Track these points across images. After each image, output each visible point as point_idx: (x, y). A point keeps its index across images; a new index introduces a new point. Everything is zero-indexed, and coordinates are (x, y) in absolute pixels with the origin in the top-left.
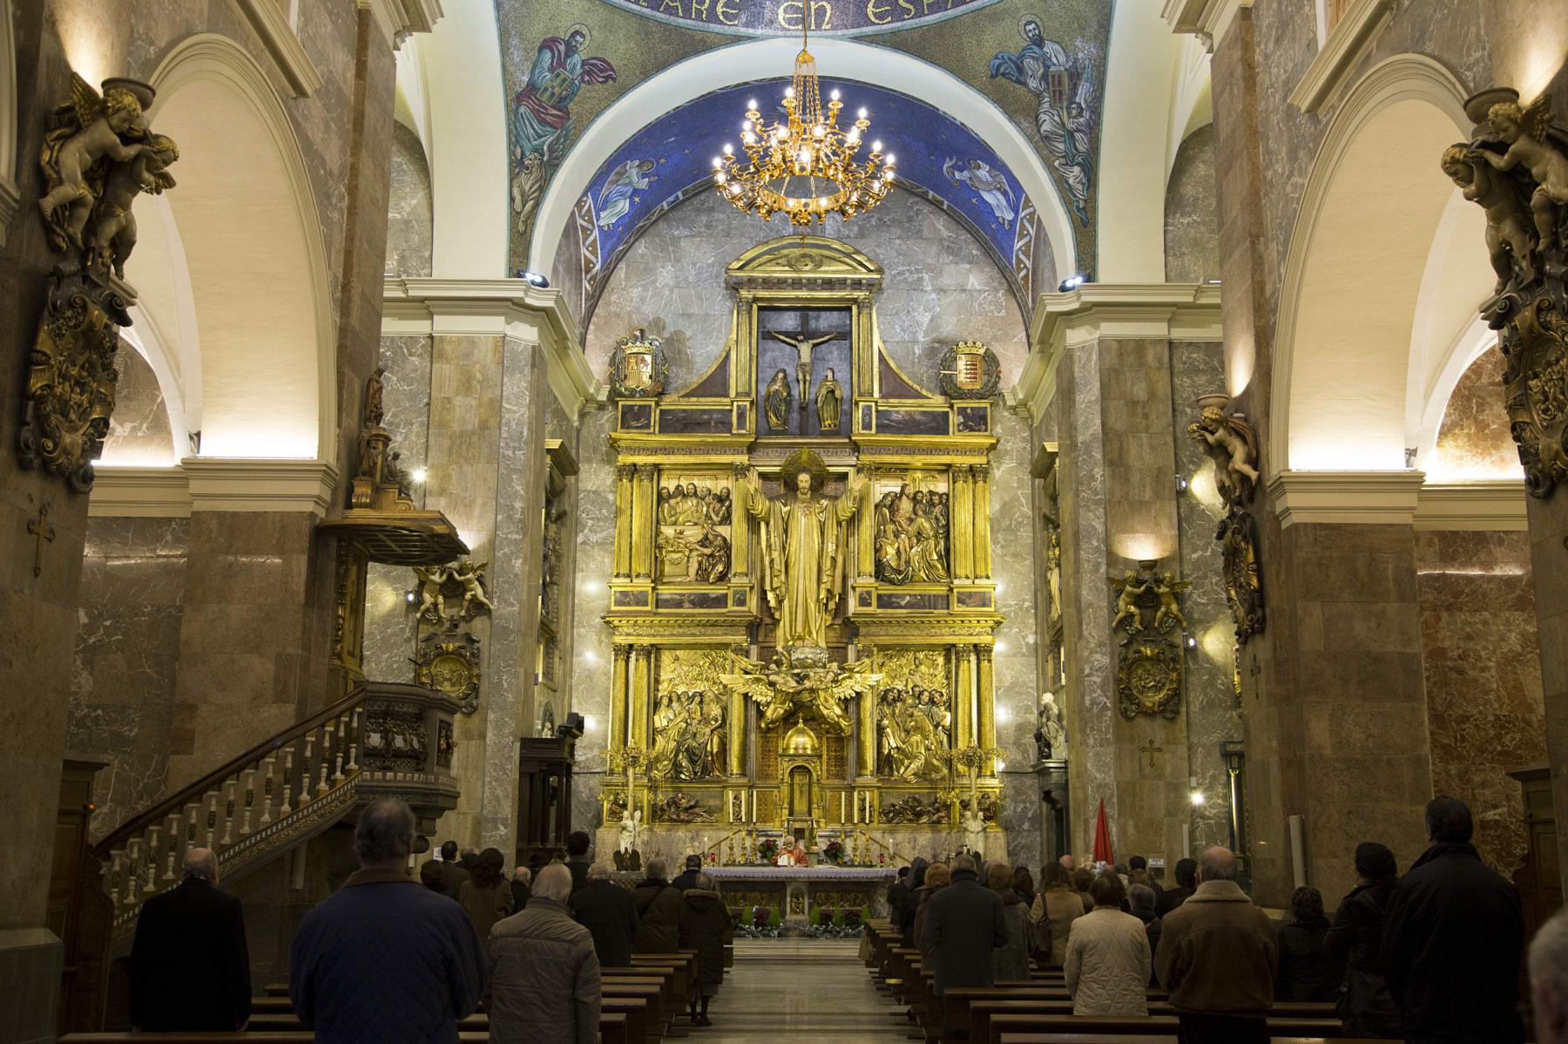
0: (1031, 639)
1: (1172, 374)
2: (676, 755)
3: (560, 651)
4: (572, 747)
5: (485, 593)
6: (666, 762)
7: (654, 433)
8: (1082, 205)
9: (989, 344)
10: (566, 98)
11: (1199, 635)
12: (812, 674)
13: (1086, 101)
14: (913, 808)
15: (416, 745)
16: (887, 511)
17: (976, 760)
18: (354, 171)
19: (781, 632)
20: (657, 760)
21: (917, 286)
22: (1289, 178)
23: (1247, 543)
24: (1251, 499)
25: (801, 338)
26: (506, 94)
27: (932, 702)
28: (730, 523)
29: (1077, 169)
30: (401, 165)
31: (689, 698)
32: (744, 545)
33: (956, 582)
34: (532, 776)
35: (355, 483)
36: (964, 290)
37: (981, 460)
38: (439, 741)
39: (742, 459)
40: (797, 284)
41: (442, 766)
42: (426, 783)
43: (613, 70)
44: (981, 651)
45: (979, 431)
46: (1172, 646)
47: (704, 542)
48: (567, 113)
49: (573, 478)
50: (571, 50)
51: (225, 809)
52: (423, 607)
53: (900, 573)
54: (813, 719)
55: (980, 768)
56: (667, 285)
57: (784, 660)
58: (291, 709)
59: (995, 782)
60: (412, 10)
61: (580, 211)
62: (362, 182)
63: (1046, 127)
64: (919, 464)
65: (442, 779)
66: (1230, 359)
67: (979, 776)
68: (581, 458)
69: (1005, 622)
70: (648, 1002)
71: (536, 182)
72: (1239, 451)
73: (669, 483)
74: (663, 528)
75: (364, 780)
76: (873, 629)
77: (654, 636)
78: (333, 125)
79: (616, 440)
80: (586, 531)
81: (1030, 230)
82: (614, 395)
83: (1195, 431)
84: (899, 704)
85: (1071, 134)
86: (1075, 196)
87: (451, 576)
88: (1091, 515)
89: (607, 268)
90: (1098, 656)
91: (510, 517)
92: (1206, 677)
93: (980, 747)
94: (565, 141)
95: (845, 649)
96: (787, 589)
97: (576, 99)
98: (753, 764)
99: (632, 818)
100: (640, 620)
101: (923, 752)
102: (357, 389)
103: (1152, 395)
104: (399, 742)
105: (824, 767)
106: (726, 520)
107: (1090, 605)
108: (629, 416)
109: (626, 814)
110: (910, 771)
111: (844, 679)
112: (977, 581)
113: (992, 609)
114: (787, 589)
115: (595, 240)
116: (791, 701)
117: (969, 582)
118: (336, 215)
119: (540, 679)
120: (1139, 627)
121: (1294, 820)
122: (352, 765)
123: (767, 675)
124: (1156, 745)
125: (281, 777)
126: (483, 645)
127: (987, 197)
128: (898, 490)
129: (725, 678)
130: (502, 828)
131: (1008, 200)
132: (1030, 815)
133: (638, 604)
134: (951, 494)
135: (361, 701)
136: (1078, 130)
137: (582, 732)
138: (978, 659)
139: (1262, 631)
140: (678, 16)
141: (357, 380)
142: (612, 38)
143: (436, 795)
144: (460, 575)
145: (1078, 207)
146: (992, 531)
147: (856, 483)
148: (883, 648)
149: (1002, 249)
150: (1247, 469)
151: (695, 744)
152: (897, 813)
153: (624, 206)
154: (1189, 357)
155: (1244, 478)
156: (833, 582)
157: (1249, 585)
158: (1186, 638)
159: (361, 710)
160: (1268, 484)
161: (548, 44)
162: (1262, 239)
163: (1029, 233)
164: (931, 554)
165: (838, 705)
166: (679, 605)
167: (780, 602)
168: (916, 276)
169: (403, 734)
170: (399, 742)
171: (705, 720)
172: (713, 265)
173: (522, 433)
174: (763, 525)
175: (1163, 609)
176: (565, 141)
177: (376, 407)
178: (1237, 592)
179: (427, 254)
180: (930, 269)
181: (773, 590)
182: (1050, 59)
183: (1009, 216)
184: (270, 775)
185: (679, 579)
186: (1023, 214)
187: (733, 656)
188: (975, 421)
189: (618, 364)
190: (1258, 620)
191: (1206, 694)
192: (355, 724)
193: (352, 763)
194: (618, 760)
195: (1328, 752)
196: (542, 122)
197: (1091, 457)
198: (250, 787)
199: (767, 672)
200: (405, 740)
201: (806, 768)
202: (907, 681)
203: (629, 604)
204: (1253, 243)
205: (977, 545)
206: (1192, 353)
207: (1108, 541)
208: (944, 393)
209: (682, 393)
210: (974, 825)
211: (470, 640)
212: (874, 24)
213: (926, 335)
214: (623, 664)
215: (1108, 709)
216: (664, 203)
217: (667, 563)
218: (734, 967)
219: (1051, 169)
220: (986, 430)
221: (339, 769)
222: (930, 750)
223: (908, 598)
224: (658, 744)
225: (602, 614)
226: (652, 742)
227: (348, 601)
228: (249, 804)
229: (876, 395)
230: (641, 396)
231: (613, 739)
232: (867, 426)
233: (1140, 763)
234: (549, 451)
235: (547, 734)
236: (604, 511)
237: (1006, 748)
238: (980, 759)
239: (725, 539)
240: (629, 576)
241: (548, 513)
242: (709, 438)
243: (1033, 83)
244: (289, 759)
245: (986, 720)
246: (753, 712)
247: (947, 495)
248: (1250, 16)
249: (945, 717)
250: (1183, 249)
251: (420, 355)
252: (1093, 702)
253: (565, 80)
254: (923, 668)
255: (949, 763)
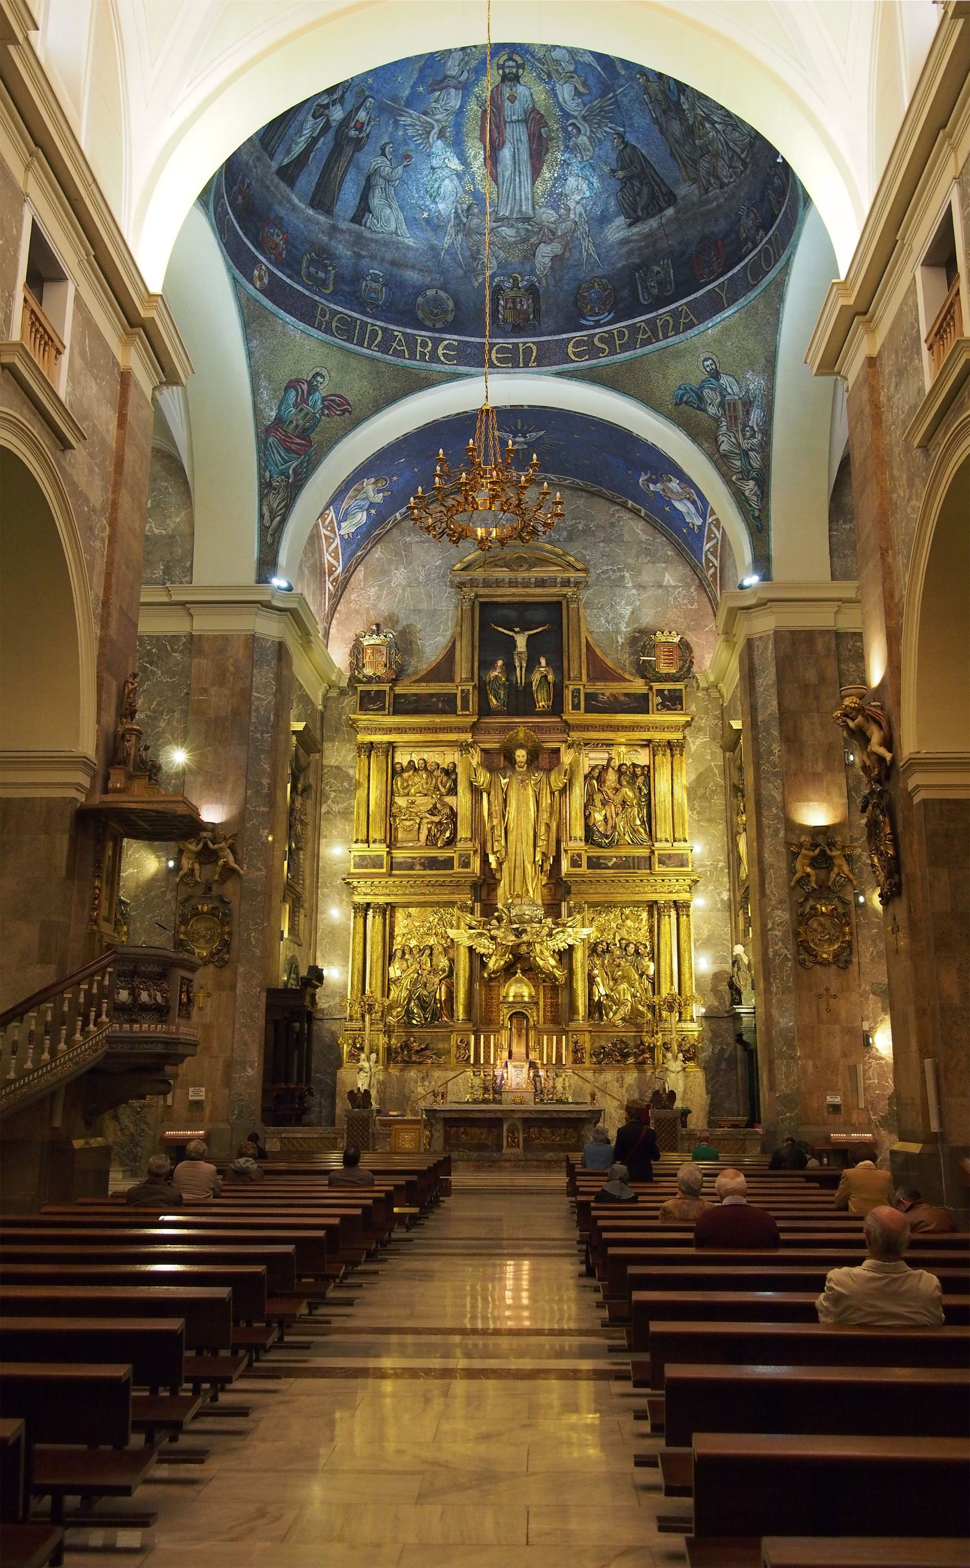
0: (725, 896)
1: (839, 661)
2: (409, 1003)
3: (305, 909)
4: (313, 996)
5: (236, 861)
6: (399, 1009)
7: (389, 715)
8: (757, 513)
9: (684, 633)
10: (308, 429)
11: (868, 893)
12: (529, 929)
13: (757, 425)
14: (621, 1050)
15: (159, 999)
16: (595, 782)
17: (676, 1004)
18: (115, 505)
19: (502, 890)
20: (391, 1007)
21: (619, 583)
22: (909, 500)
23: (884, 816)
24: (888, 777)
25: (517, 629)
26: (257, 428)
27: (637, 952)
28: (456, 794)
29: (752, 483)
30: (167, 488)
31: (420, 950)
32: (469, 813)
33: (657, 845)
34: (276, 1023)
35: (112, 771)
36: (661, 586)
37: (674, 736)
38: (180, 996)
39: (468, 737)
40: (513, 583)
41: (183, 1017)
42: (168, 1033)
43: (349, 404)
44: (680, 907)
45: (675, 710)
46: (845, 903)
47: (433, 811)
48: (310, 442)
49: (317, 756)
50: (312, 389)
51: (9, 1050)
52: (181, 873)
53: (607, 837)
54: (531, 969)
55: (680, 1013)
56: (400, 584)
57: (505, 917)
58: (52, 968)
59: (694, 1026)
60: (167, 369)
61: (323, 523)
62: (121, 515)
63: (724, 447)
64: (623, 740)
65: (183, 1029)
66: (868, 654)
67: (680, 1021)
68: (325, 738)
69: (701, 881)
70: (327, 1234)
71: (283, 501)
72: (876, 736)
73: (402, 758)
74: (397, 800)
75: (115, 1031)
76: (584, 887)
77: (389, 895)
78: (96, 469)
79: (355, 721)
80: (330, 802)
81: (717, 533)
82: (353, 680)
83: (839, 718)
84: (607, 956)
85: (746, 453)
86: (751, 506)
87: (206, 844)
88: (770, 785)
89: (348, 571)
90: (779, 912)
91: (258, 792)
92: (875, 931)
93: (680, 994)
94: (308, 465)
95: (559, 905)
96: (506, 852)
97: (317, 429)
98: (477, 1012)
99: (368, 1059)
100: (376, 881)
101: (629, 998)
102: (114, 690)
103: (822, 679)
104: (144, 997)
105: (541, 1013)
106: (453, 791)
107: (771, 866)
108: (366, 700)
109: (363, 1056)
110: (618, 1016)
111: (557, 933)
112: (675, 844)
113: (689, 869)
114: (506, 852)
115: (337, 547)
116: (511, 953)
117: (669, 845)
118: (98, 544)
119: (286, 935)
120: (815, 886)
121: (928, 1062)
122: (104, 1018)
123: (489, 930)
124: (832, 992)
125: (42, 1029)
126: (235, 905)
127: (678, 505)
128: (605, 763)
129: (452, 933)
130: (250, 1070)
131: (697, 509)
132: (726, 1056)
133: (374, 867)
134: (652, 766)
135: (112, 962)
136: (752, 450)
137: (322, 983)
138: (678, 914)
139: (899, 894)
140: (405, 358)
141: (114, 683)
142: (348, 378)
143: (177, 1044)
144: (214, 844)
145: (753, 516)
146: (689, 799)
147: (567, 758)
148: (593, 905)
149: (692, 550)
150: (882, 751)
151: (425, 993)
152: (607, 1055)
153: (362, 517)
154: (853, 646)
155: (881, 759)
156: (548, 845)
157: (887, 853)
158: (856, 896)
159: (111, 970)
160: (901, 764)
161: (293, 384)
162: (890, 552)
163: (716, 537)
164: (634, 820)
165: (553, 956)
166: (412, 867)
167: (500, 864)
168: (618, 574)
169: (148, 990)
170: (144, 997)
171: (434, 971)
172: (440, 566)
173: (269, 718)
174: (485, 795)
175: (836, 869)
176: (308, 465)
177: (130, 704)
178: (879, 859)
179: (188, 564)
180: (628, 567)
181: (494, 853)
182: (726, 389)
183: (699, 522)
184: (33, 1028)
185: (411, 844)
186: (710, 520)
187: (459, 913)
188: (673, 701)
189: (357, 651)
190: (895, 884)
191: (875, 946)
192: (106, 982)
193: (104, 1017)
194: (356, 1007)
195: (957, 1001)
196: (288, 450)
197: (769, 734)
198: (16, 1038)
199: (489, 927)
200: (150, 996)
201: (523, 1014)
202: (614, 935)
203: (367, 868)
204: (882, 555)
205: (675, 811)
206: (856, 642)
207: (785, 808)
208: (644, 677)
209: (414, 678)
210: (675, 1065)
211: (221, 899)
212: (574, 361)
213: (628, 625)
214: (362, 920)
215: (788, 960)
216: (398, 514)
217: (400, 830)
218: (452, 1197)
219: (728, 482)
220: (682, 709)
221: (92, 1022)
222: (635, 997)
223: (614, 859)
224: (392, 992)
225: (344, 876)
226: (386, 992)
227: (104, 875)
228: (14, 1053)
229: (584, 678)
230: (377, 682)
231: (352, 988)
232: (576, 707)
233: (818, 1010)
234: (294, 732)
235: (293, 985)
236: (346, 784)
237: (704, 995)
238: (680, 1005)
239: (451, 809)
240: (367, 841)
241: (294, 788)
242: (438, 719)
243: (712, 410)
244: (49, 1013)
245: (685, 970)
246: (478, 964)
247: (649, 767)
248: (875, 365)
249: (649, 967)
250: (847, 551)
251: (181, 652)
252: (776, 954)
253: (307, 414)
254: (629, 923)
255: (652, 1008)
